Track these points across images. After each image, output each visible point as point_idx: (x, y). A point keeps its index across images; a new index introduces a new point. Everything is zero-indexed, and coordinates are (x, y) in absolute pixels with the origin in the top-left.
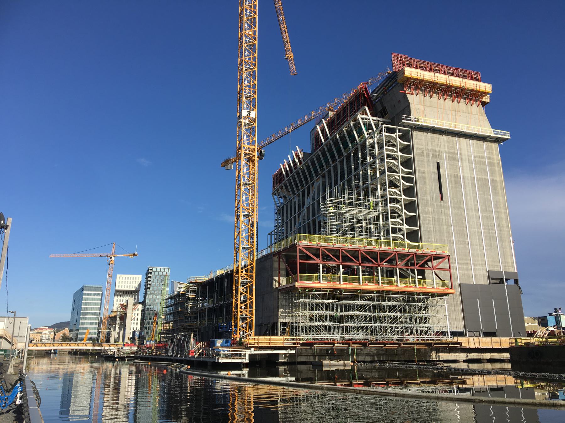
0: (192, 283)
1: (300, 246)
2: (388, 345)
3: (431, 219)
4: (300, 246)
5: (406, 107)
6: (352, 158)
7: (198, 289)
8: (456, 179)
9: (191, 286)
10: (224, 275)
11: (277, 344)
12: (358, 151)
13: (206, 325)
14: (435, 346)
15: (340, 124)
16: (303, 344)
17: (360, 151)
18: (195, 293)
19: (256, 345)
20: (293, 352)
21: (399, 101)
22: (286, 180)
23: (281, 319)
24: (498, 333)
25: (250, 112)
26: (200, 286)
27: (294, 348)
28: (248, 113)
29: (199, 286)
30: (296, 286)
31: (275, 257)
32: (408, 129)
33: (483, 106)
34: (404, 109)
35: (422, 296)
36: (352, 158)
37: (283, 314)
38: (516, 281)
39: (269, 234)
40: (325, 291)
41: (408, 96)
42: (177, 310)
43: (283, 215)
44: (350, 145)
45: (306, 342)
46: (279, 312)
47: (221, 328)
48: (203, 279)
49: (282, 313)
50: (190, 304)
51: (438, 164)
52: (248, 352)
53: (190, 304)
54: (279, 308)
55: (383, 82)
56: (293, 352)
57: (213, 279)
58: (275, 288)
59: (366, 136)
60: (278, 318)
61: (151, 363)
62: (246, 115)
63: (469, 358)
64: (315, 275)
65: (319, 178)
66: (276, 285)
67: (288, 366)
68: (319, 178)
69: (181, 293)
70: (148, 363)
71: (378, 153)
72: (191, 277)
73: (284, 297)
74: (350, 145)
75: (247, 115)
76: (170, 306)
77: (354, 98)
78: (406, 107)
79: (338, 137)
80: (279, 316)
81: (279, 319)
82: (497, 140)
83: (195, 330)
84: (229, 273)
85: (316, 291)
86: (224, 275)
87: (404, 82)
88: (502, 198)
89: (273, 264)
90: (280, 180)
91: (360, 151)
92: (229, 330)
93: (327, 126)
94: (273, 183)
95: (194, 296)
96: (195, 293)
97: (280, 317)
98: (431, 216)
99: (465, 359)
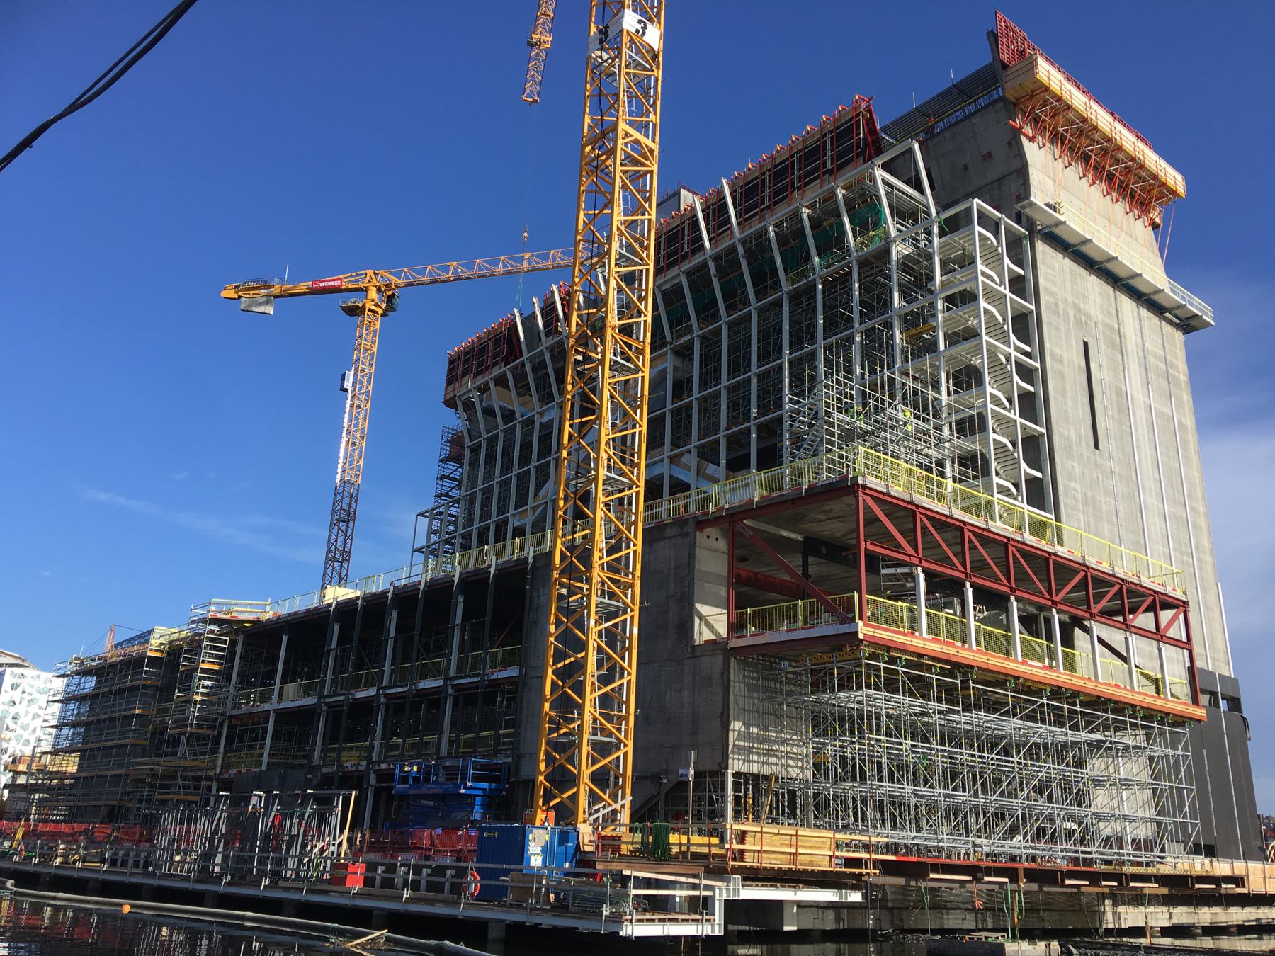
0: (214, 621)
1: (867, 491)
2: (989, 875)
3: (1079, 496)
4: (867, 491)
5: (1010, 174)
6: (819, 297)
7: (233, 643)
8: (1122, 397)
9: (212, 632)
10: (390, 595)
11: (811, 863)
12: (849, 274)
13: (264, 767)
14: (1132, 884)
15: (781, 195)
16: (887, 868)
17: (856, 276)
18: (221, 657)
19: (749, 861)
20: (856, 897)
21: (988, 156)
22: (524, 358)
23: (736, 761)
24: (1218, 849)
25: (645, 25)
26: (242, 636)
27: (856, 883)
28: (639, 27)
29: (236, 632)
30: (861, 636)
31: (701, 531)
32: (1023, 230)
33: (1154, 229)
34: (1000, 179)
35: (1142, 719)
36: (819, 297)
37: (742, 743)
38: (1235, 704)
39: (422, 515)
40: (929, 668)
41: (1024, 140)
42: (131, 712)
43: (474, 464)
44: (817, 260)
45: (893, 858)
46: (731, 734)
47: (404, 780)
48: (248, 610)
49: (739, 738)
50: (204, 687)
51: (1086, 345)
52: (722, 891)
53: (204, 687)
54: (731, 718)
55: (927, 103)
56: (856, 897)
57: (383, 594)
58: (697, 643)
59: (893, 233)
60: (727, 758)
61: (132, 906)
62: (634, 31)
63: (1175, 921)
64: (900, 604)
65: (666, 353)
66: (702, 634)
67: (765, 947)
68: (666, 353)
69: (149, 654)
70: (121, 905)
71: (942, 282)
72: (214, 600)
73: (744, 677)
74: (817, 260)
75: (637, 31)
76: (80, 699)
77: (825, 136)
78: (1010, 174)
79: (772, 234)
80: (730, 747)
81: (730, 761)
82: (1187, 324)
83: (203, 783)
84: (422, 587)
85: (909, 664)
86: (390, 595)
87: (1017, 99)
88: (1192, 472)
89: (692, 557)
90: (480, 365)
91: (856, 276)
92: (463, 791)
93: (703, 211)
94: (448, 374)
95: (216, 667)
96: (221, 657)
97: (733, 753)
98: (1078, 488)
99: (1167, 924)
